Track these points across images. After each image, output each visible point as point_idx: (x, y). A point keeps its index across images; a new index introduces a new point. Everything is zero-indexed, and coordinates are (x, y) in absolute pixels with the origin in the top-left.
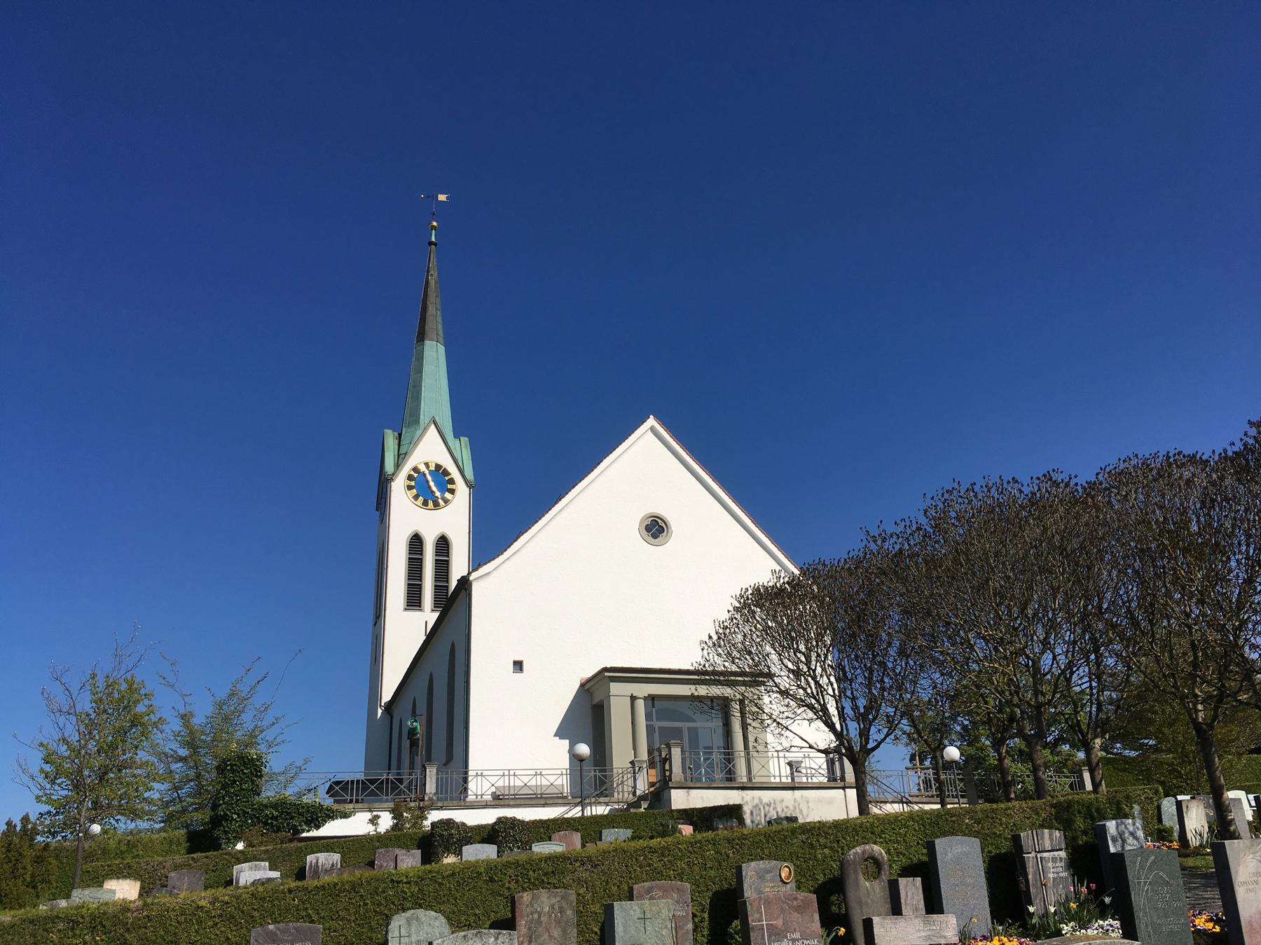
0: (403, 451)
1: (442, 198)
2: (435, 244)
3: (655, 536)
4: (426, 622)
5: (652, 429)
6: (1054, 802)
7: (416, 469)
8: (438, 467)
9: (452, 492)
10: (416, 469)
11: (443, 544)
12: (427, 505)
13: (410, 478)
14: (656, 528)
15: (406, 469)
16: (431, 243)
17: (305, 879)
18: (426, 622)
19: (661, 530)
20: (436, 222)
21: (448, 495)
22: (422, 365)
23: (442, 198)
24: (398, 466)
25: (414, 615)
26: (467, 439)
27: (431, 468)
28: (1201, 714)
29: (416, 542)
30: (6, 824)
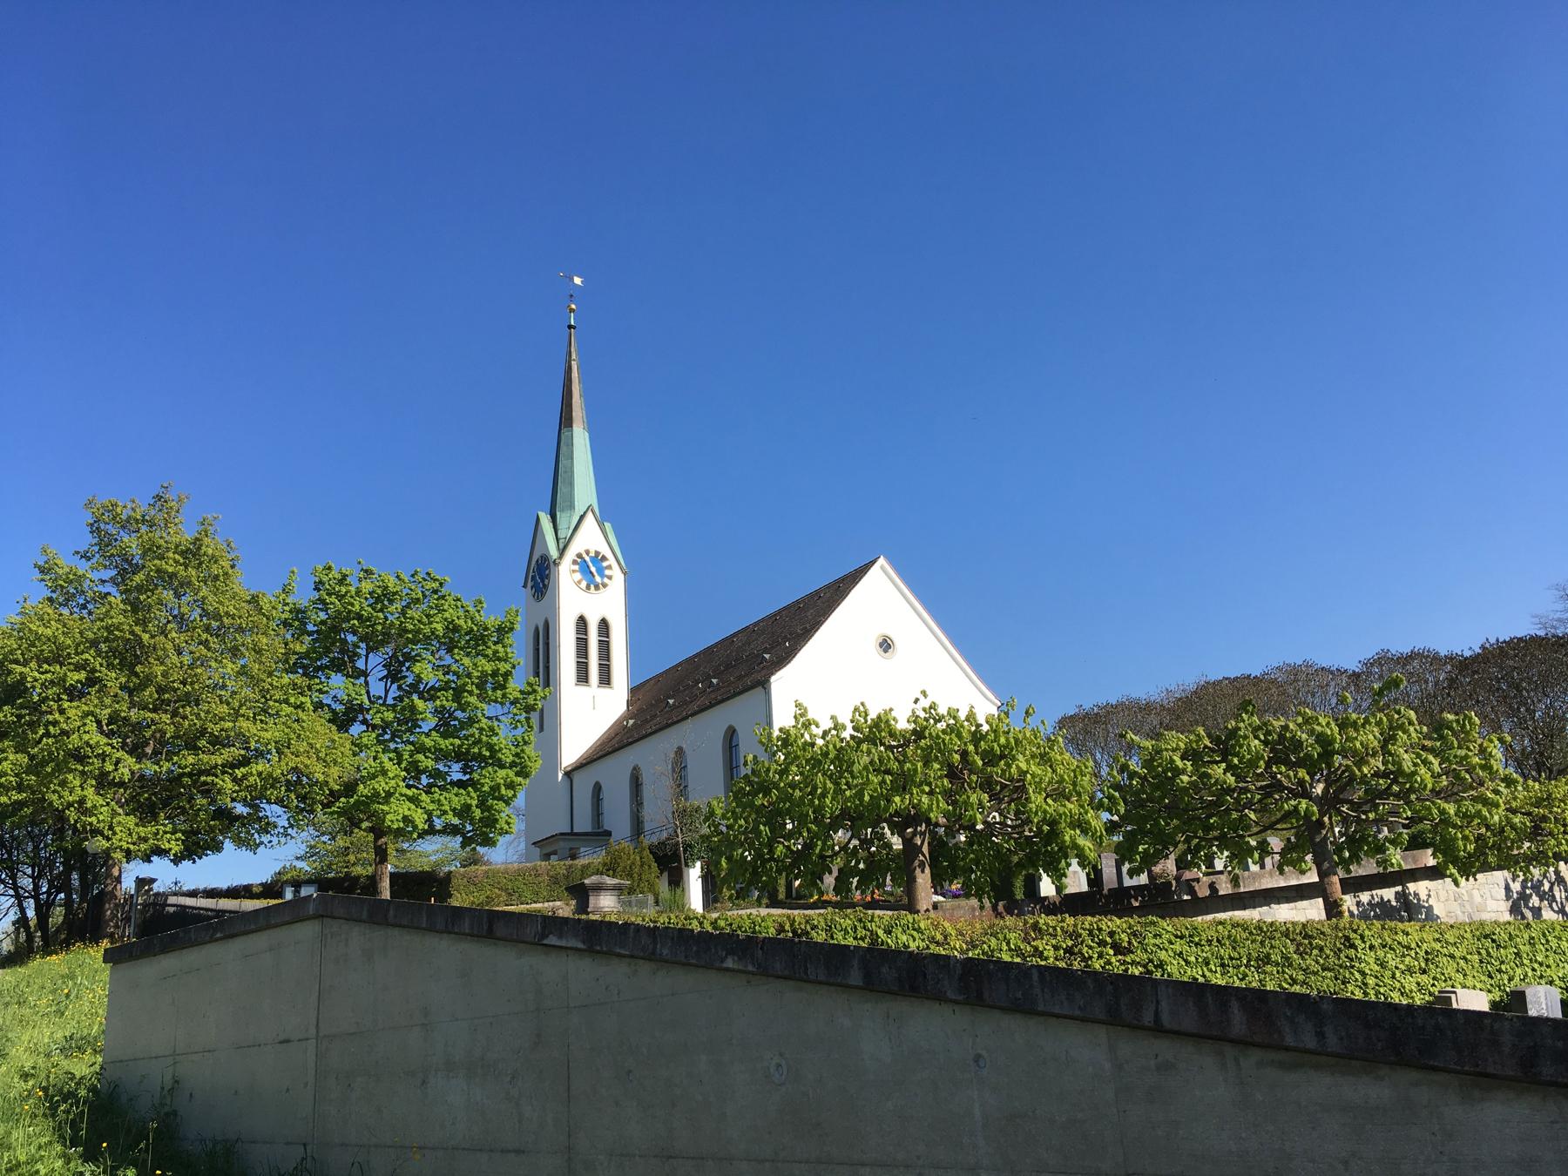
0: (562, 534)
1: (577, 281)
2: (574, 328)
3: (886, 651)
4: (594, 708)
5: (882, 568)
6: (1064, 1119)
7: (579, 556)
8: (597, 553)
9: (610, 578)
10: (579, 556)
11: (604, 626)
12: (589, 589)
13: (575, 562)
14: (886, 645)
15: (571, 554)
16: (570, 327)
17: (104, 962)
18: (594, 708)
19: (889, 646)
20: (575, 305)
21: (606, 580)
22: (572, 452)
23: (577, 281)
24: (562, 552)
25: (583, 689)
26: (609, 525)
27: (590, 555)
28: (896, 819)
29: (582, 623)
30: (150, 861)
